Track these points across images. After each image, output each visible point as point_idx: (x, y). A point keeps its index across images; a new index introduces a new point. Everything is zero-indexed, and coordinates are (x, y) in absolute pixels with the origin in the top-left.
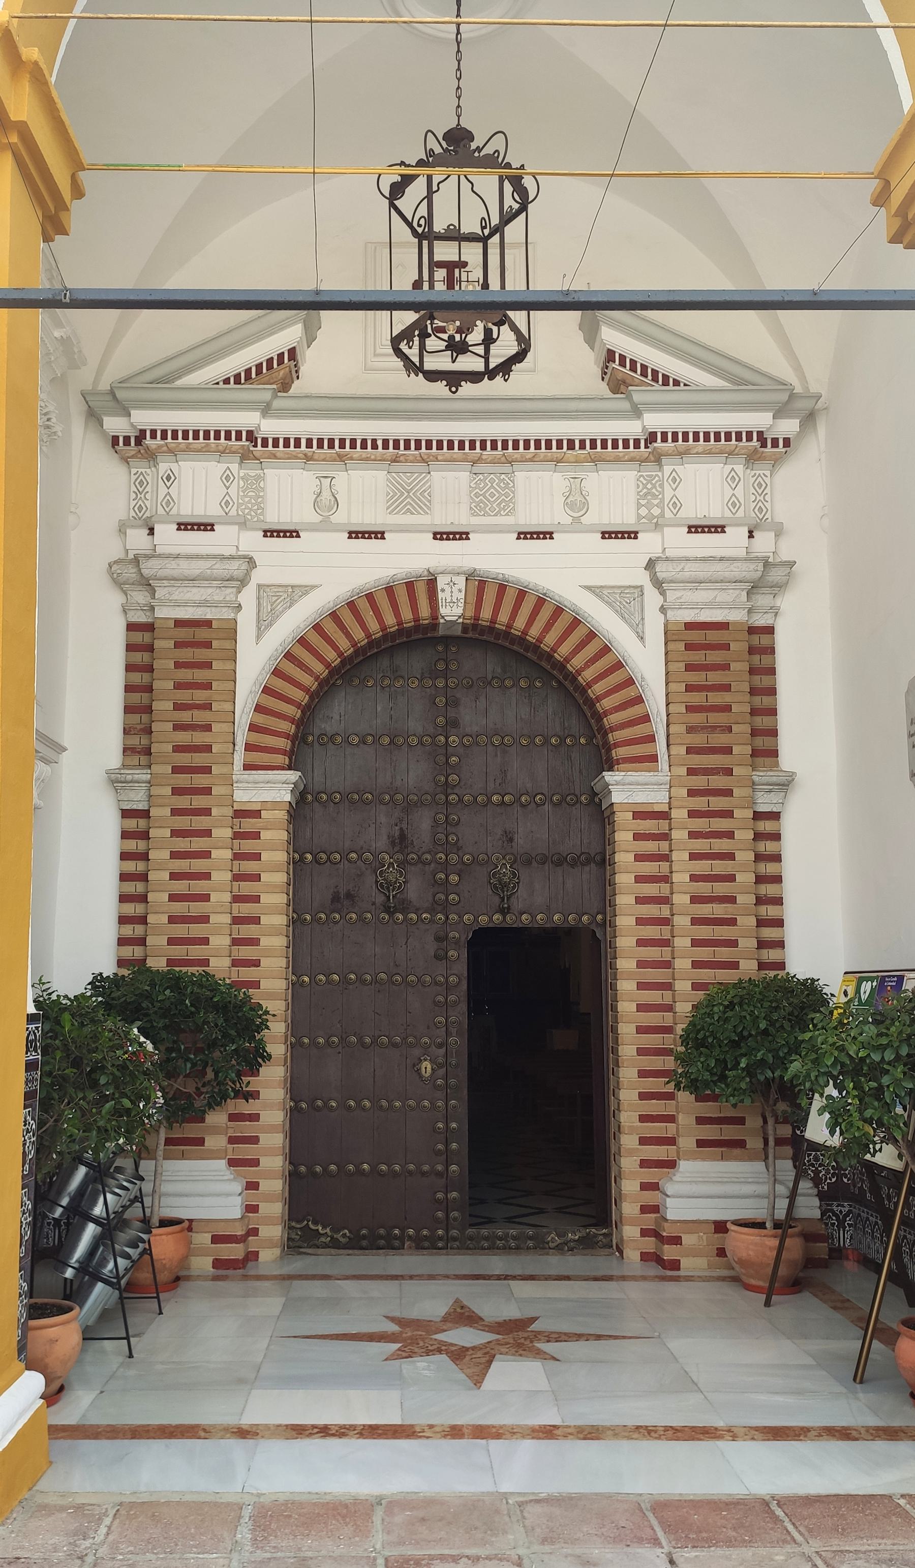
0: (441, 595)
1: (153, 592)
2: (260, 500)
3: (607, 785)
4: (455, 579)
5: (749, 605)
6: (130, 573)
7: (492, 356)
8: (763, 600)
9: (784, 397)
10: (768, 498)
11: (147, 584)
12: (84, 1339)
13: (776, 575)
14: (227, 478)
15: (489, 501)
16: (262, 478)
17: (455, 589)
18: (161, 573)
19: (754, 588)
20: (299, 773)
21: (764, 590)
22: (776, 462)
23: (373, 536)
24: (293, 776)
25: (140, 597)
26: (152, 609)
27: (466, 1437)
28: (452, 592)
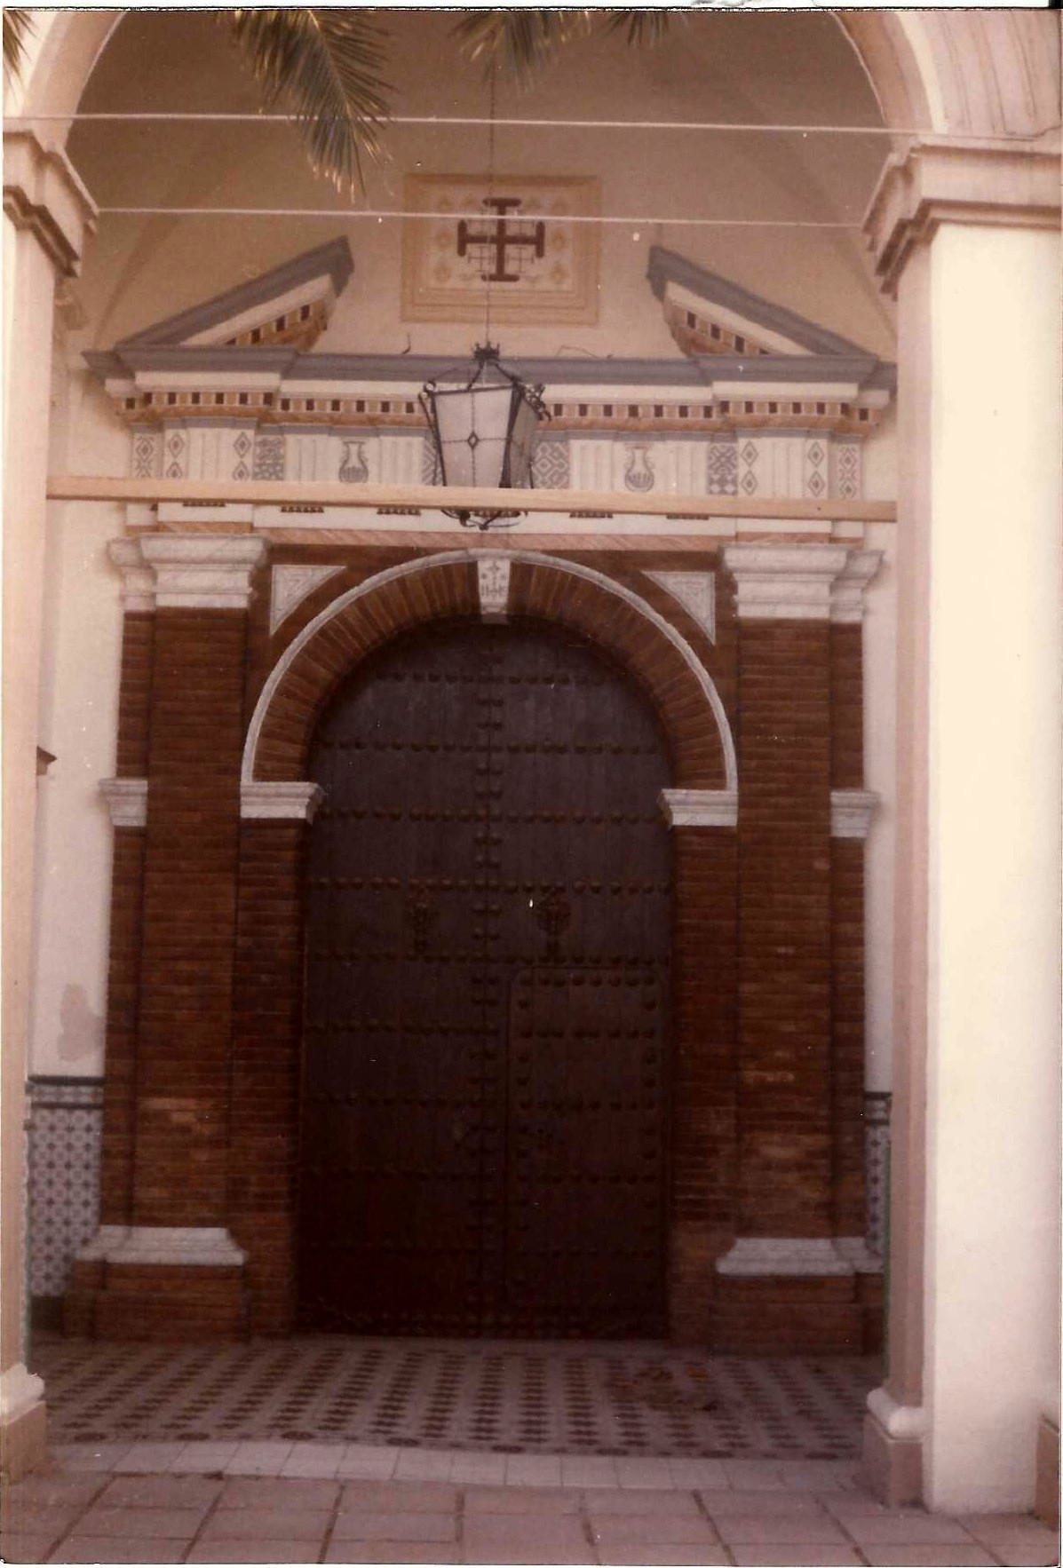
0: (481, 582)
1: (154, 576)
2: (278, 468)
3: (667, 804)
4: (499, 564)
5: (831, 600)
6: (127, 554)
7: (395, 443)
8: (850, 595)
9: (869, 368)
10: (857, 475)
11: (147, 567)
12: (50, 497)
13: (865, 565)
14: (241, 445)
15: (551, 469)
16: (282, 443)
17: (498, 574)
18: (166, 555)
19: (839, 580)
20: (316, 785)
21: (851, 583)
22: (865, 438)
23: (407, 511)
24: (307, 788)
25: (139, 583)
26: (153, 596)
27: (118, 863)
28: (495, 578)
